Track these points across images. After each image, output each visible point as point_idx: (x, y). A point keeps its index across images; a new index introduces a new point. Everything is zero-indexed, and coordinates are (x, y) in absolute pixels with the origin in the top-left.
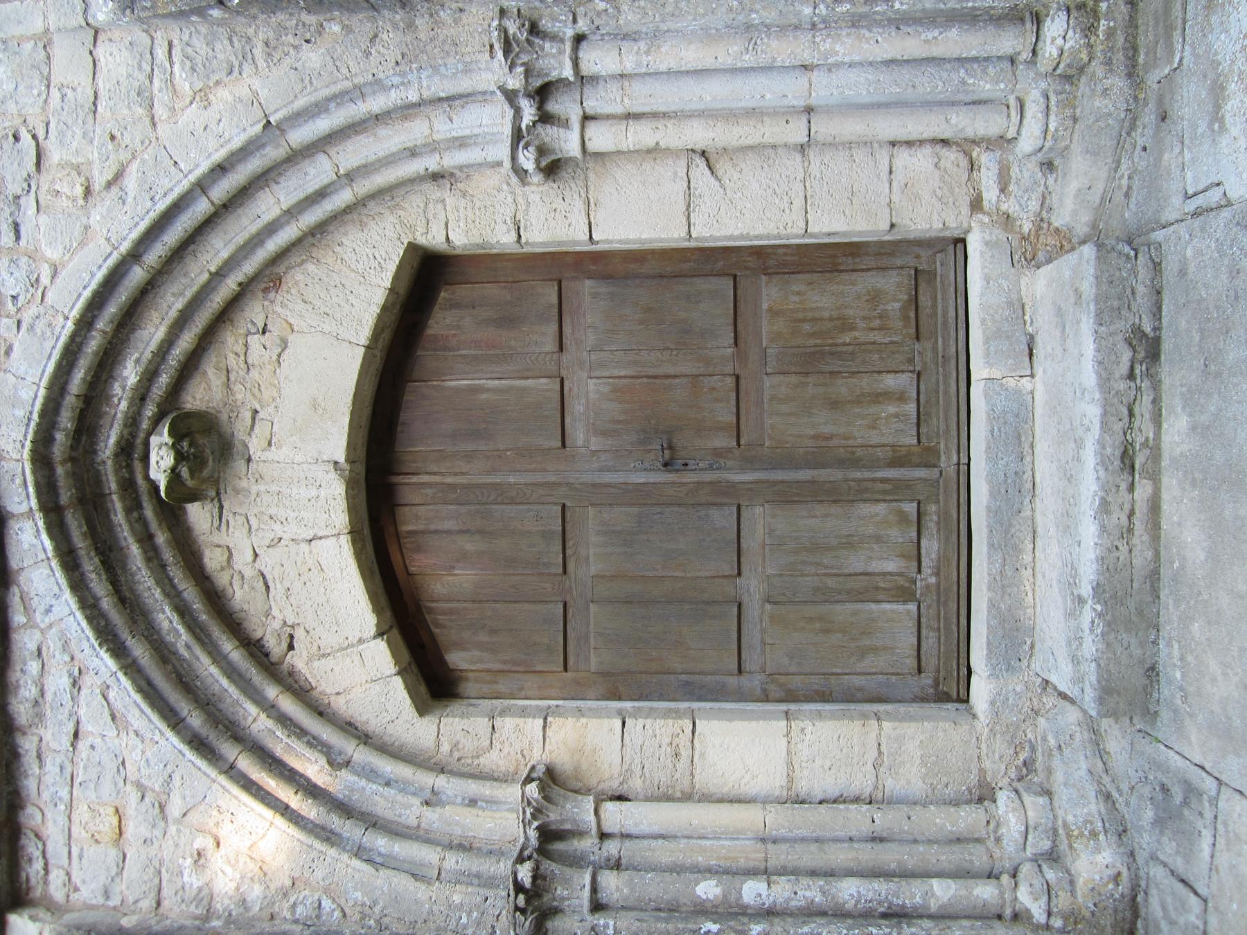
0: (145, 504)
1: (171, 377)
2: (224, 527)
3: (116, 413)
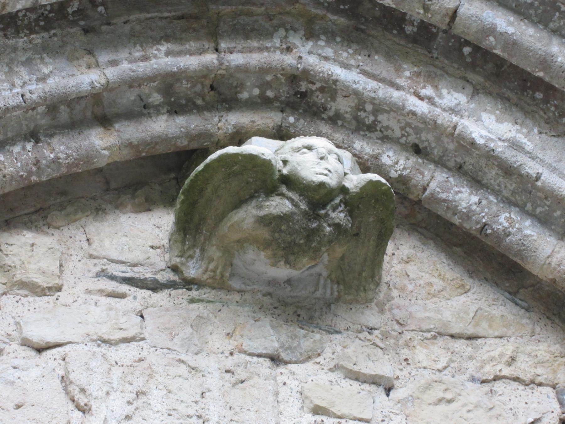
0: (180, 120)
1: (467, 216)
2: (111, 286)
3: (398, 88)
